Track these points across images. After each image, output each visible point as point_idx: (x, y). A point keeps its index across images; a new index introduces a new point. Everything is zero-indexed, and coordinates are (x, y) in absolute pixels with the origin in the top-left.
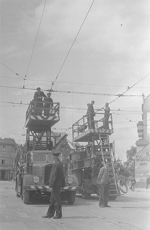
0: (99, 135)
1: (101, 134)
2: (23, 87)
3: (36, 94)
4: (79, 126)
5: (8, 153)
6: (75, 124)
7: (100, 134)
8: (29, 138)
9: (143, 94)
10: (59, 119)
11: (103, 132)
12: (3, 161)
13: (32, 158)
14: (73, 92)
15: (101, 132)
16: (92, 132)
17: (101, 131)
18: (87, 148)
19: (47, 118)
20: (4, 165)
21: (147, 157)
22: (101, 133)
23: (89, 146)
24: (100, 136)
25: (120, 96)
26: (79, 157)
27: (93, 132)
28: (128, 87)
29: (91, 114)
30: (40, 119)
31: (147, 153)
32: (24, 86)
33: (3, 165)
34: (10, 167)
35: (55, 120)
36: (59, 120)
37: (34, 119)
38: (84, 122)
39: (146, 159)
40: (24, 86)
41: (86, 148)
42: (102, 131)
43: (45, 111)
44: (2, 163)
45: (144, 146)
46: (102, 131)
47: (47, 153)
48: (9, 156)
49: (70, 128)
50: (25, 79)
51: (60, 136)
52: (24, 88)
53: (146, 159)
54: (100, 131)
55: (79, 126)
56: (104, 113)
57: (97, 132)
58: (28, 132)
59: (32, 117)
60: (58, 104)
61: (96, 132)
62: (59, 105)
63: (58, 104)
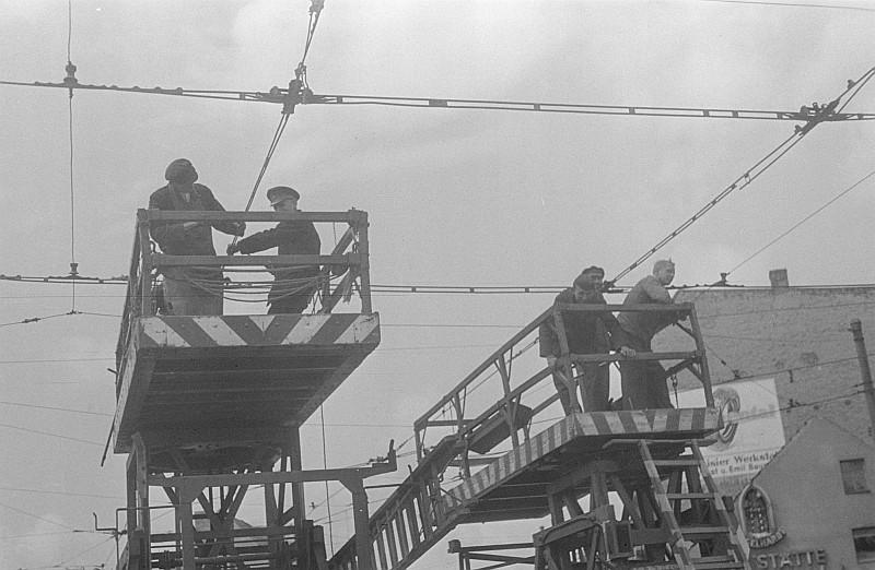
2: (68, 271)
3: (159, 199)
7: (644, 442)
8: (145, 501)
9: (724, 275)
15: (647, 429)
18: (547, 552)
19: (280, 328)
25: (813, 122)
27: (591, 430)
32: (74, 266)
35: (346, 338)
36: (372, 343)
37: (177, 340)
38: (506, 380)
40: (74, 266)
49: (411, 453)
51: (392, 467)
52: (74, 276)
56: (521, 403)
58: (135, 483)
59: (160, 331)
60: (358, 220)
63: (358, 220)
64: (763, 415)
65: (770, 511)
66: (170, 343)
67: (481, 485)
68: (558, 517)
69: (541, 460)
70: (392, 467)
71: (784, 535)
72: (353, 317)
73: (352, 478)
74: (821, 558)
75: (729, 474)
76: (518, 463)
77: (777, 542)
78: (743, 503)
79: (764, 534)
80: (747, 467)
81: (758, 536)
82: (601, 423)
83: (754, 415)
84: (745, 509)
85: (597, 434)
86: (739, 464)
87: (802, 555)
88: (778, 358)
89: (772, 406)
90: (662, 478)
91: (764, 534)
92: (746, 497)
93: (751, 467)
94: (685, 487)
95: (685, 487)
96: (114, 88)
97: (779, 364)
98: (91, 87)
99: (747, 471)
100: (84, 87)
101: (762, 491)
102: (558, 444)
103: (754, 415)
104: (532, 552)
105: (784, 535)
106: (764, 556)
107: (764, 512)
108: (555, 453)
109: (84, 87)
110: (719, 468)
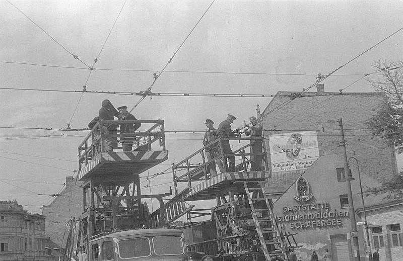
0: (243, 184)
1: (247, 182)
4: (191, 169)
5: (11, 229)
6: (181, 165)
7: (245, 182)
10: (167, 155)
11: (251, 177)
12: (3, 244)
13: (117, 250)
14: (179, 95)
15: (247, 178)
16: (228, 179)
17: (246, 175)
18: (215, 214)
20: (7, 253)
21: (285, 215)
22: (246, 180)
23: (218, 209)
24: (245, 185)
26: (199, 234)
27: (229, 178)
28: (320, 74)
29: (222, 141)
30: (124, 159)
31: (284, 209)
33: (4, 253)
34: (17, 255)
37: (112, 159)
39: (283, 220)
41: (214, 212)
42: (248, 175)
43: (318, 132)
44: (3, 250)
45: (278, 196)
46: (248, 175)
47: (152, 235)
48: (13, 236)
50: (92, 69)
51: (170, 194)
53: (283, 220)
54: (235, 175)
55: (191, 169)
57: (239, 178)
61: (236, 178)
62: (163, 124)
64: (311, 145)
65: (308, 188)
66: (110, 160)
67: (195, 191)
68: (219, 202)
69: (214, 186)
70: (170, 194)
71: (313, 197)
72: (160, 152)
73: (159, 197)
74: (327, 206)
75: (296, 169)
76: (207, 186)
77: (310, 200)
78: (298, 184)
79: (305, 197)
80: (303, 167)
81: (303, 197)
82: (233, 176)
83: (307, 145)
84: (299, 186)
85: (231, 179)
86: (300, 165)
87: (320, 205)
88: (319, 122)
89: (315, 142)
90: (250, 192)
91: (305, 197)
92: (299, 181)
93: (305, 167)
94: (258, 196)
95: (258, 196)
96: (97, 92)
97: (319, 124)
98: (90, 92)
99: (303, 168)
100: (88, 92)
101: (306, 179)
102: (219, 181)
103: (307, 145)
104: (210, 212)
105: (313, 197)
106: (304, 205)
107: (306, 188)
108: (218, 184)
109: (88, 92)
110: (292, 166)
